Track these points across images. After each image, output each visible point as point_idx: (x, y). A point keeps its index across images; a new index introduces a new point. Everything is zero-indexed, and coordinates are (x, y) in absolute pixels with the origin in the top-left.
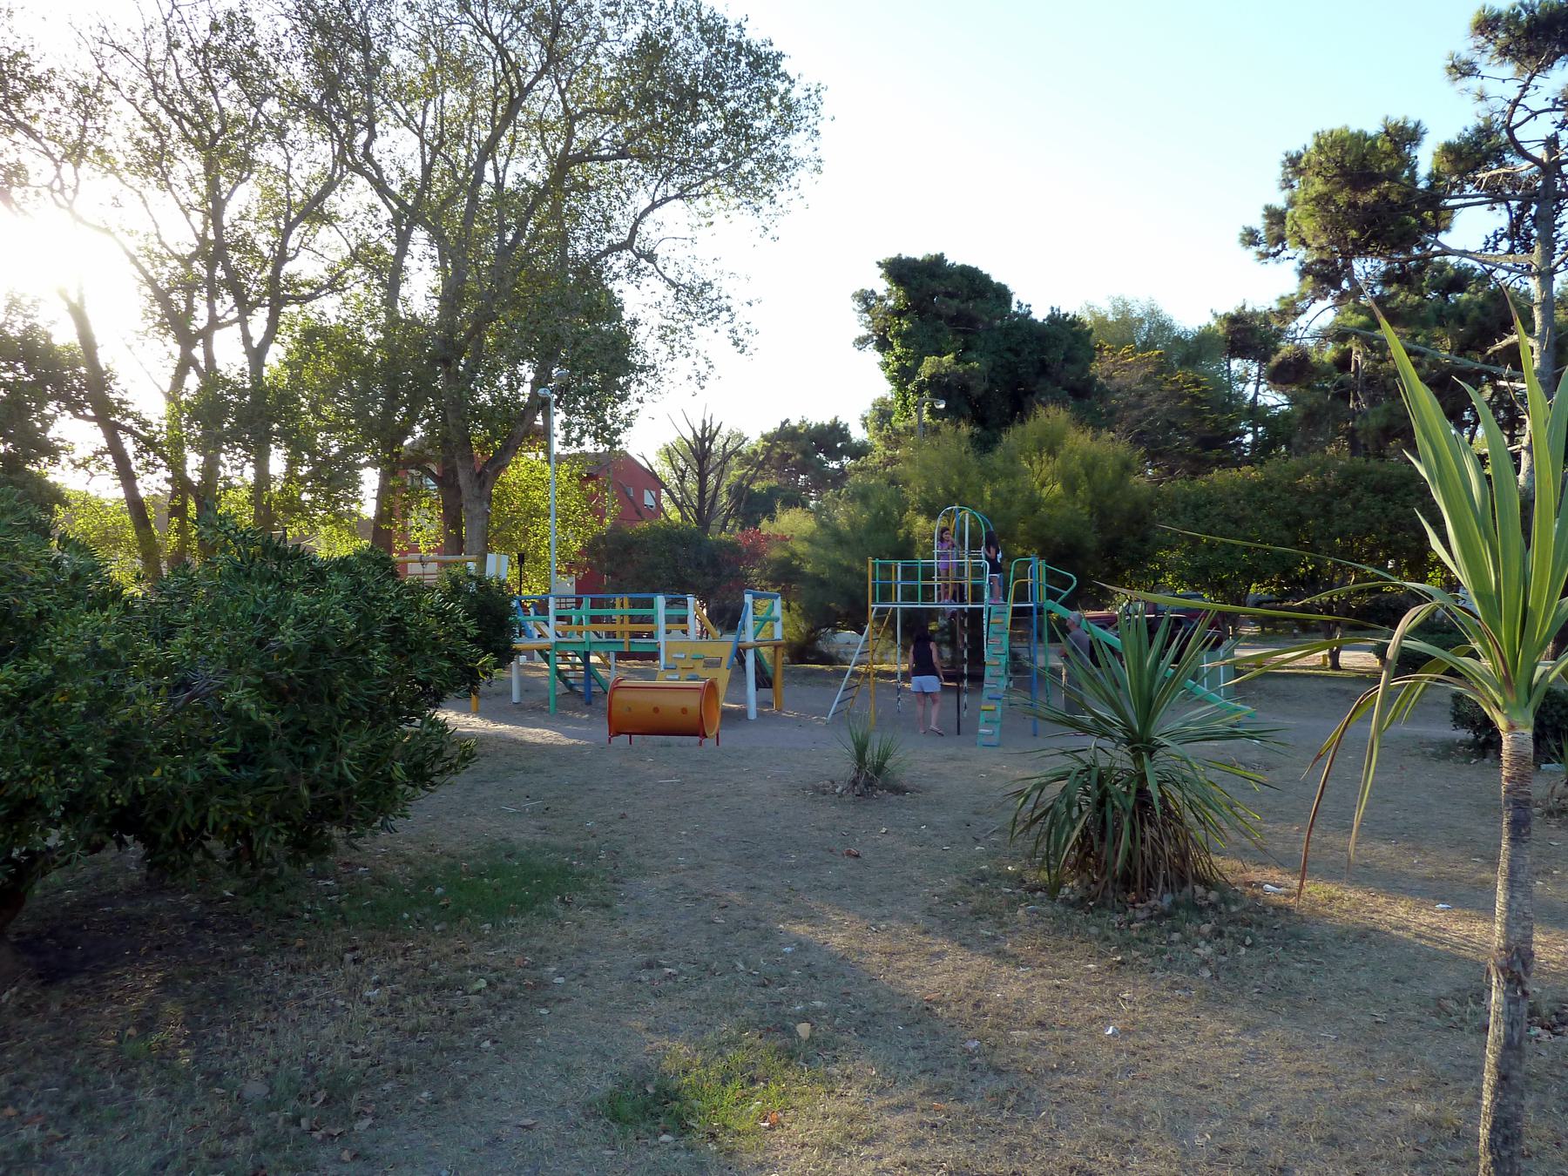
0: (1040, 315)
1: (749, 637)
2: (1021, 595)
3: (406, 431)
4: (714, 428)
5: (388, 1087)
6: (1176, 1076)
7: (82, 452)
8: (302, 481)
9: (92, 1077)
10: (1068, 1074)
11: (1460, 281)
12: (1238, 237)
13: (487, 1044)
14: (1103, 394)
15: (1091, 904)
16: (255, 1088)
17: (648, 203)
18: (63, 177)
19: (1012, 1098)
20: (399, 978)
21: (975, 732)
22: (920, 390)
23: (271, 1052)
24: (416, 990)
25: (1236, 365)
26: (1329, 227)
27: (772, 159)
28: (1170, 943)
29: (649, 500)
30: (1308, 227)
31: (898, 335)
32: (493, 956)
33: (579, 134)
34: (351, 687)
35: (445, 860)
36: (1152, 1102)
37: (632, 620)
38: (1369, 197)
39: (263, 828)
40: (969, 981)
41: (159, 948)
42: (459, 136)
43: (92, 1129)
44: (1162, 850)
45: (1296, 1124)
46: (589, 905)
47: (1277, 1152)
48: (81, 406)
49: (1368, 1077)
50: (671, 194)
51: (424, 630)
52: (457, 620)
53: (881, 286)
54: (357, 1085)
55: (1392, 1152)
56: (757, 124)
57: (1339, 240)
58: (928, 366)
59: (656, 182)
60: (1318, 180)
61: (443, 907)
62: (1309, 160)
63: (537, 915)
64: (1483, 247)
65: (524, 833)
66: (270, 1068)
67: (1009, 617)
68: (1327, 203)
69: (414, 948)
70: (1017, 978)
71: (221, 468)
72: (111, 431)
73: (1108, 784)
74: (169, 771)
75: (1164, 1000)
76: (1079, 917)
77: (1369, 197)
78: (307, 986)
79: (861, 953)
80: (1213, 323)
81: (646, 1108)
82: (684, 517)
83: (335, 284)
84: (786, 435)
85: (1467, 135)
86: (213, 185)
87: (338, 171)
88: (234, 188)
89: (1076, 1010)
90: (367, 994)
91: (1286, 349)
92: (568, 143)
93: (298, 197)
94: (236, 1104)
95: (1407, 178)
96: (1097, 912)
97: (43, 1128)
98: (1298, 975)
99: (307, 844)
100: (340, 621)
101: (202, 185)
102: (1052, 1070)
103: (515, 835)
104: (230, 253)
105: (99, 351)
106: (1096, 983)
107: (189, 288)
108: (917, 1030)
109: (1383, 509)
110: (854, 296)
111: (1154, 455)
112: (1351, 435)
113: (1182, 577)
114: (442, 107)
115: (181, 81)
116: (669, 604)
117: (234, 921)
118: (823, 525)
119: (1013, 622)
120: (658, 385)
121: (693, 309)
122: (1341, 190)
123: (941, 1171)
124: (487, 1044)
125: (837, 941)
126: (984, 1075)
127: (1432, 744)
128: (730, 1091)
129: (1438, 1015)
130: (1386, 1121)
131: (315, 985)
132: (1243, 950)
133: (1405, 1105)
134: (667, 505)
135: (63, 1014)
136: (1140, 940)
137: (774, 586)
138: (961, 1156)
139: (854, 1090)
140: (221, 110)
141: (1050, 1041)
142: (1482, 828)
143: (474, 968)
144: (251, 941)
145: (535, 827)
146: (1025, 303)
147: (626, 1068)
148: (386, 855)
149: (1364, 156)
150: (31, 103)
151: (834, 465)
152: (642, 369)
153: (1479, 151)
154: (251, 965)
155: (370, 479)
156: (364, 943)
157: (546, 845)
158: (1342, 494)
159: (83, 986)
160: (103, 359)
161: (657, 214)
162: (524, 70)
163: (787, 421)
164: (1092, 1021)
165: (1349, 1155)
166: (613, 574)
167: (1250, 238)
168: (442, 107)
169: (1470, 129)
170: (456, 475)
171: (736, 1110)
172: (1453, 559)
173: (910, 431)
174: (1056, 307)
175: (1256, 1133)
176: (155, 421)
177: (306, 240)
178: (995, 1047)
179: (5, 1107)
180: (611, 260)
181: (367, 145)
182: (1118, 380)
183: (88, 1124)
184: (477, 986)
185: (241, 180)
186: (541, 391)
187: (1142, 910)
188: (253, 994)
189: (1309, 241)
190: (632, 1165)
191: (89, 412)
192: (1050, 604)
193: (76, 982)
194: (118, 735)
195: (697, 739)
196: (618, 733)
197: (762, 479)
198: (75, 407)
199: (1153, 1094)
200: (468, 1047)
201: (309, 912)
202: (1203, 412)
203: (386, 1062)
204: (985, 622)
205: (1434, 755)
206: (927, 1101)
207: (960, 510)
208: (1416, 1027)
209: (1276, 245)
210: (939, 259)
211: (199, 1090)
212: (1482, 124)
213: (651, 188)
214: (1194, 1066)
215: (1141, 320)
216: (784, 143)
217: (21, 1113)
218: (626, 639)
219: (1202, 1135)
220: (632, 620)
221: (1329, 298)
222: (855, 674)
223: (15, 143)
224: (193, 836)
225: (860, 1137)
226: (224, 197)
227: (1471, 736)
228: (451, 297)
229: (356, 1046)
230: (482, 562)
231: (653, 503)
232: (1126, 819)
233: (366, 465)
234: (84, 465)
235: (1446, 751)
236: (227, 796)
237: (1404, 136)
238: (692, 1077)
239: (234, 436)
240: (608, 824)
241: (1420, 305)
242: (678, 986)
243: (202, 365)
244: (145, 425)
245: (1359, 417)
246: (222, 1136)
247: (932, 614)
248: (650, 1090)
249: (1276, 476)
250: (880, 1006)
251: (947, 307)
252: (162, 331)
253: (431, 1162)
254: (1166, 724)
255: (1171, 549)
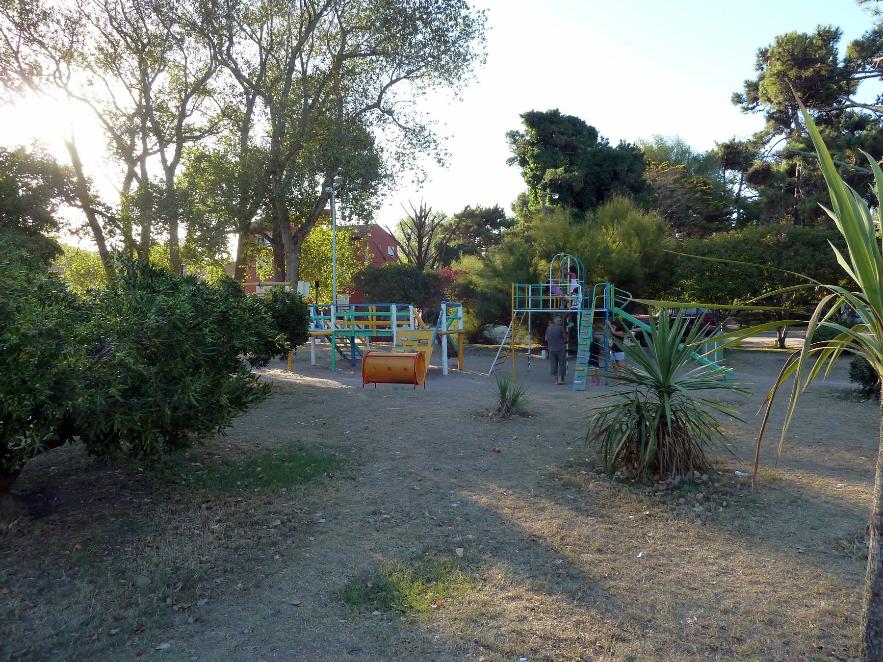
0: (614, 144)
1: (444, 329)
2: (600, 304)
3: (253, 213)
4: (427, 210)
5: (219, 581)
6: (678, 582)
7: (75, 226)
8: (196, 241)
9: (53, 572)
10: (614, 580)
11: (861, 123)
12: (731, 99)
13: (278, 557)
14: (650, 189)
15: (633, 481)
16: (143, 581)
17: (389, 81)
18: (61, 69)
19: (580, 594)
20: (231, 518)
21: (572, 383)
22: (544, 188)
23: (155, 559)
24: (240, 525)
25: (729, 174)
26: (785, 91)
27: (459, 54)
28: (678, 504)
29: (390, 252)
30: (772, 91)
31: (532, 156)
32: (286, 507)
33: (349, 42)
34: (194, 351)
35: (264, 452)
36: (663, 598)
37: (378, 318)
38: (809, 73)
39: (148, 432)
40: (559, 525)
41: (100, 500)
42: (281, 43)
43: (49, 602)
44: (676, 450)
45: (748, 612)
46: (344, 478)
47: (736, 629)
48: (74, 199)
49: (793, 585)
50: (402, 75)
51: (242, 319)
52: (260, 313)
53: (522, 128)
54: (201, 579)
55: (806, 630)
56: (450, 34)
57: (790, 98)
58: (549, 175)
59: (393, 69)
60: (778, 63)
61: (261, 478)
62: (773, 52)
63: (313, 483)
64: (876, 102)
65: (310, 437)
66: (153, 568)
67: (592, 317)
68: (783, 77)
69: (242, 501)
70: (587, 523)
71: (151, 234)
72: (91, 213)
73: (643, 412)
74: (87, 399)
75: (674, 537)
76: (625, 489)
77: (809, 73)
78: (179, 522)
79: (498, 508)
80: (716, 149)
81: (366, 595)
82: (410, 261)
83: (212, 130)
84: (468, 215)
85: (867, 35)
86: (144, 74)
87: (214, 65)
88: (156, 75)
89: (621, 542)
90: (213, 527)
91: (757, 163)
92: (343, 48)
93: (191, 80)
94: (131, 588)
95: (831, 61)
96: (636, 486)
97: (23, 600)
98: (753, 524)
99: (176, 443)
100: (184, 312)
101: (138, 73)
102: (605, 578)
103: (304, 439)
104: (154, 112)
105: (83, 168)
106: (633, 527)
107: (132, 133)
108: (526, 553)
109: (813, 256)
110: (507, 134)
111: (679, 225)
112: (796, 214)
113: (694, 295)
114: (271, 27)
115: (125, 14)
116: (398, 310)
117: (142, 485)
118: (486, 265)
119: (594, 320)
120: (394, 185)
121: (415, 142)
122: (792, 69)
123: (535, 636)
124: (278, 557)
125: (484, 500)
126: (564, 579)
127: (838, 391)
128: (415, 587)
129: (836, 549)
130: (802, 612)
131: (184, 521)
132: (721, 509)
133: (815, 602)
134: (401, 254)
135: (41, 536)
136: (661, 502)
137: (459, 300)
138: (548, 627)
139: (488, 587)
140: (147, 30)
141: (604, 560)
142: (866, 440)
143: (275, 513)
144: (150, 496)
145: (317, 434)
146: (605, 137)
147: (356, 572)
148: (231, 449)
149: (806, 48)
150: (42, 27)
151: (496, 232)
152: (385, 176)
153: (874, 45)
154: (149, 509)
155: (233, 241)
156: (213, 498)
157: (321, 444)
158: (787, 246)
159: (54, 520)
160: (86, 173)
161: (393, 88)
162: (318, 5)
163: (469, 206)
164: (630, 549)
165: (780, 631)
166: (370, 293)
167: (738, 99)
168: (271, 27)
169: (869, 32)
170: (281, 237)
171: (418, 598)
172: (854, 272)
173: (538, 211)
174: (623, 140)
175: (724, 617)
176: (114, 208)
177: (197, 105)
178: (572, 563)
179: (3, 588)
180: (368, 114)
181: (228, 50)
182: (659, 182)
183: (48, 599)
184: (275, 524)
185: (160, 71)
186: (327, 189)
187: (662, 484)
188: (148, 526)
189: (773, 99)
190: (355, 629)
191: (79, 203)
192: (616, 310)
193: (51, 518)
194: (58, 377)
195: (413, 385)
196: (369, 382)
197: (455, 240)
198: (69, 200)
199: (664, 593)
200: (267, 559)
201: (185, 480)
202: (708, 200)
203: (219, 566)
204: (578, 320)
205: (839, 397)
206: (530, 595)
207: (565, 256)
208: (823, 555)
209: (753, 103)
210: (556, 113)
211: (111, 580)
212: (876, 28)
213: (390, 73)
214: (689, 577)
215: (673, 148)
216: (465, 45)
217: (11, 592)
218: (375, 329)
219: (692, 618)
220: (378, 318)
221: (784, 134)
222: (504, 349)
223: (34, 51)
224: (111, 438)
225: (489, 615)
226: (150, 80)
227: (861, 387)
228: (277, 134)
229: (203, 557)
230: (295, 287)
231: (393, 254)
232: (652, 433)
233: (230, 232)
234: (76, 232)
235: (846, 395)
236: (125, 413)
237: (830, 36)
238: (394, 578)
239: (157, 217)
240: (357, 432)
241: (837, 137)
242: (390, 525)
243: (140, 176)
244: (108, 209)
245: (800, 203)
246: (122, 607)
247: (550, 316)
248: (370, 585)
249: (749, 236)
250: (506, 539)
251: (561, 140)
252: (118, 157)
253: (239, 625)
254: (682, 375)
255: (687, 278)
